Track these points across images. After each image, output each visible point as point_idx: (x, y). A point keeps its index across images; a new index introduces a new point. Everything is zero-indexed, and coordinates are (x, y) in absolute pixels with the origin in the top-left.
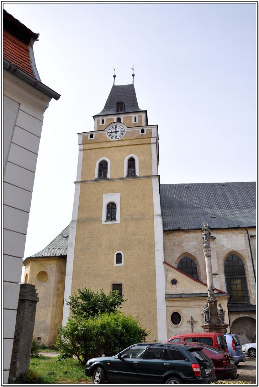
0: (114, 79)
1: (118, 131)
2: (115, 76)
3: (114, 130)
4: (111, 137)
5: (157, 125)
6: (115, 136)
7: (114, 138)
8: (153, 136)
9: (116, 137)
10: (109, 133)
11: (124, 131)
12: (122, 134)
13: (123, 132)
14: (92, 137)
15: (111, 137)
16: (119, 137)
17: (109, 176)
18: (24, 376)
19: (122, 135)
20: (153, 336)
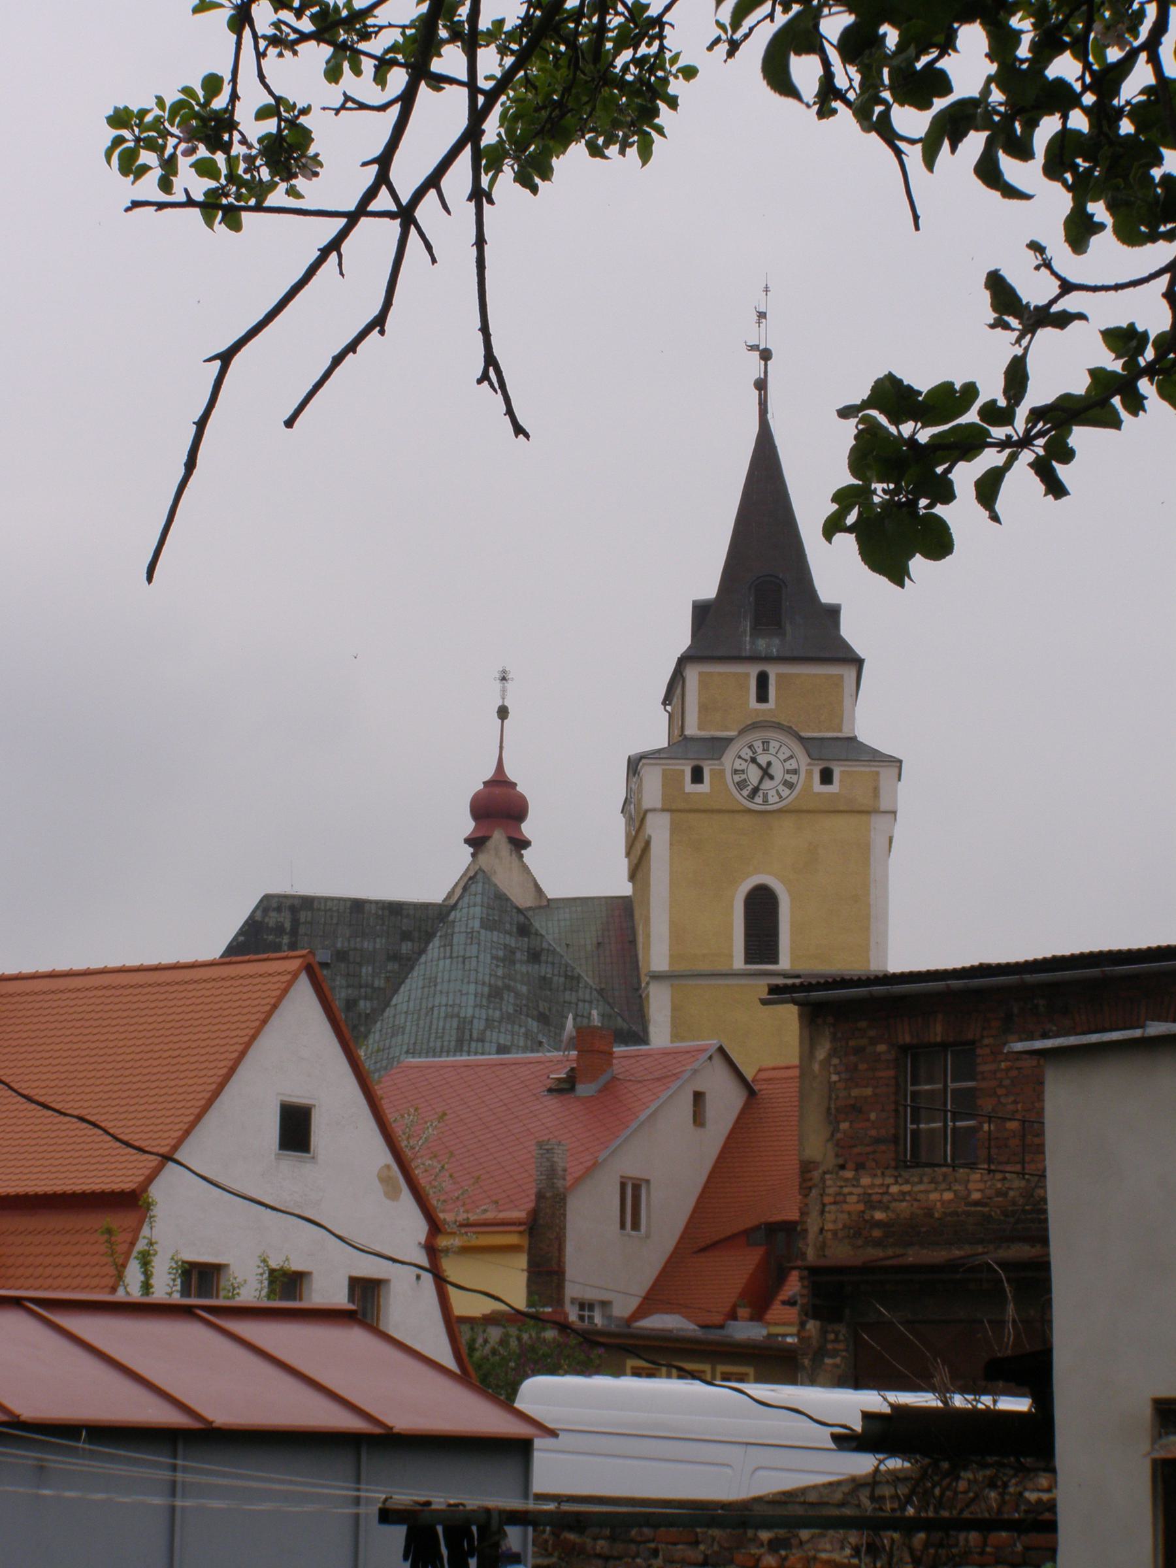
0: (766, 365)
1: (769, 764)
8: (882, 809)
19: (787, 792)
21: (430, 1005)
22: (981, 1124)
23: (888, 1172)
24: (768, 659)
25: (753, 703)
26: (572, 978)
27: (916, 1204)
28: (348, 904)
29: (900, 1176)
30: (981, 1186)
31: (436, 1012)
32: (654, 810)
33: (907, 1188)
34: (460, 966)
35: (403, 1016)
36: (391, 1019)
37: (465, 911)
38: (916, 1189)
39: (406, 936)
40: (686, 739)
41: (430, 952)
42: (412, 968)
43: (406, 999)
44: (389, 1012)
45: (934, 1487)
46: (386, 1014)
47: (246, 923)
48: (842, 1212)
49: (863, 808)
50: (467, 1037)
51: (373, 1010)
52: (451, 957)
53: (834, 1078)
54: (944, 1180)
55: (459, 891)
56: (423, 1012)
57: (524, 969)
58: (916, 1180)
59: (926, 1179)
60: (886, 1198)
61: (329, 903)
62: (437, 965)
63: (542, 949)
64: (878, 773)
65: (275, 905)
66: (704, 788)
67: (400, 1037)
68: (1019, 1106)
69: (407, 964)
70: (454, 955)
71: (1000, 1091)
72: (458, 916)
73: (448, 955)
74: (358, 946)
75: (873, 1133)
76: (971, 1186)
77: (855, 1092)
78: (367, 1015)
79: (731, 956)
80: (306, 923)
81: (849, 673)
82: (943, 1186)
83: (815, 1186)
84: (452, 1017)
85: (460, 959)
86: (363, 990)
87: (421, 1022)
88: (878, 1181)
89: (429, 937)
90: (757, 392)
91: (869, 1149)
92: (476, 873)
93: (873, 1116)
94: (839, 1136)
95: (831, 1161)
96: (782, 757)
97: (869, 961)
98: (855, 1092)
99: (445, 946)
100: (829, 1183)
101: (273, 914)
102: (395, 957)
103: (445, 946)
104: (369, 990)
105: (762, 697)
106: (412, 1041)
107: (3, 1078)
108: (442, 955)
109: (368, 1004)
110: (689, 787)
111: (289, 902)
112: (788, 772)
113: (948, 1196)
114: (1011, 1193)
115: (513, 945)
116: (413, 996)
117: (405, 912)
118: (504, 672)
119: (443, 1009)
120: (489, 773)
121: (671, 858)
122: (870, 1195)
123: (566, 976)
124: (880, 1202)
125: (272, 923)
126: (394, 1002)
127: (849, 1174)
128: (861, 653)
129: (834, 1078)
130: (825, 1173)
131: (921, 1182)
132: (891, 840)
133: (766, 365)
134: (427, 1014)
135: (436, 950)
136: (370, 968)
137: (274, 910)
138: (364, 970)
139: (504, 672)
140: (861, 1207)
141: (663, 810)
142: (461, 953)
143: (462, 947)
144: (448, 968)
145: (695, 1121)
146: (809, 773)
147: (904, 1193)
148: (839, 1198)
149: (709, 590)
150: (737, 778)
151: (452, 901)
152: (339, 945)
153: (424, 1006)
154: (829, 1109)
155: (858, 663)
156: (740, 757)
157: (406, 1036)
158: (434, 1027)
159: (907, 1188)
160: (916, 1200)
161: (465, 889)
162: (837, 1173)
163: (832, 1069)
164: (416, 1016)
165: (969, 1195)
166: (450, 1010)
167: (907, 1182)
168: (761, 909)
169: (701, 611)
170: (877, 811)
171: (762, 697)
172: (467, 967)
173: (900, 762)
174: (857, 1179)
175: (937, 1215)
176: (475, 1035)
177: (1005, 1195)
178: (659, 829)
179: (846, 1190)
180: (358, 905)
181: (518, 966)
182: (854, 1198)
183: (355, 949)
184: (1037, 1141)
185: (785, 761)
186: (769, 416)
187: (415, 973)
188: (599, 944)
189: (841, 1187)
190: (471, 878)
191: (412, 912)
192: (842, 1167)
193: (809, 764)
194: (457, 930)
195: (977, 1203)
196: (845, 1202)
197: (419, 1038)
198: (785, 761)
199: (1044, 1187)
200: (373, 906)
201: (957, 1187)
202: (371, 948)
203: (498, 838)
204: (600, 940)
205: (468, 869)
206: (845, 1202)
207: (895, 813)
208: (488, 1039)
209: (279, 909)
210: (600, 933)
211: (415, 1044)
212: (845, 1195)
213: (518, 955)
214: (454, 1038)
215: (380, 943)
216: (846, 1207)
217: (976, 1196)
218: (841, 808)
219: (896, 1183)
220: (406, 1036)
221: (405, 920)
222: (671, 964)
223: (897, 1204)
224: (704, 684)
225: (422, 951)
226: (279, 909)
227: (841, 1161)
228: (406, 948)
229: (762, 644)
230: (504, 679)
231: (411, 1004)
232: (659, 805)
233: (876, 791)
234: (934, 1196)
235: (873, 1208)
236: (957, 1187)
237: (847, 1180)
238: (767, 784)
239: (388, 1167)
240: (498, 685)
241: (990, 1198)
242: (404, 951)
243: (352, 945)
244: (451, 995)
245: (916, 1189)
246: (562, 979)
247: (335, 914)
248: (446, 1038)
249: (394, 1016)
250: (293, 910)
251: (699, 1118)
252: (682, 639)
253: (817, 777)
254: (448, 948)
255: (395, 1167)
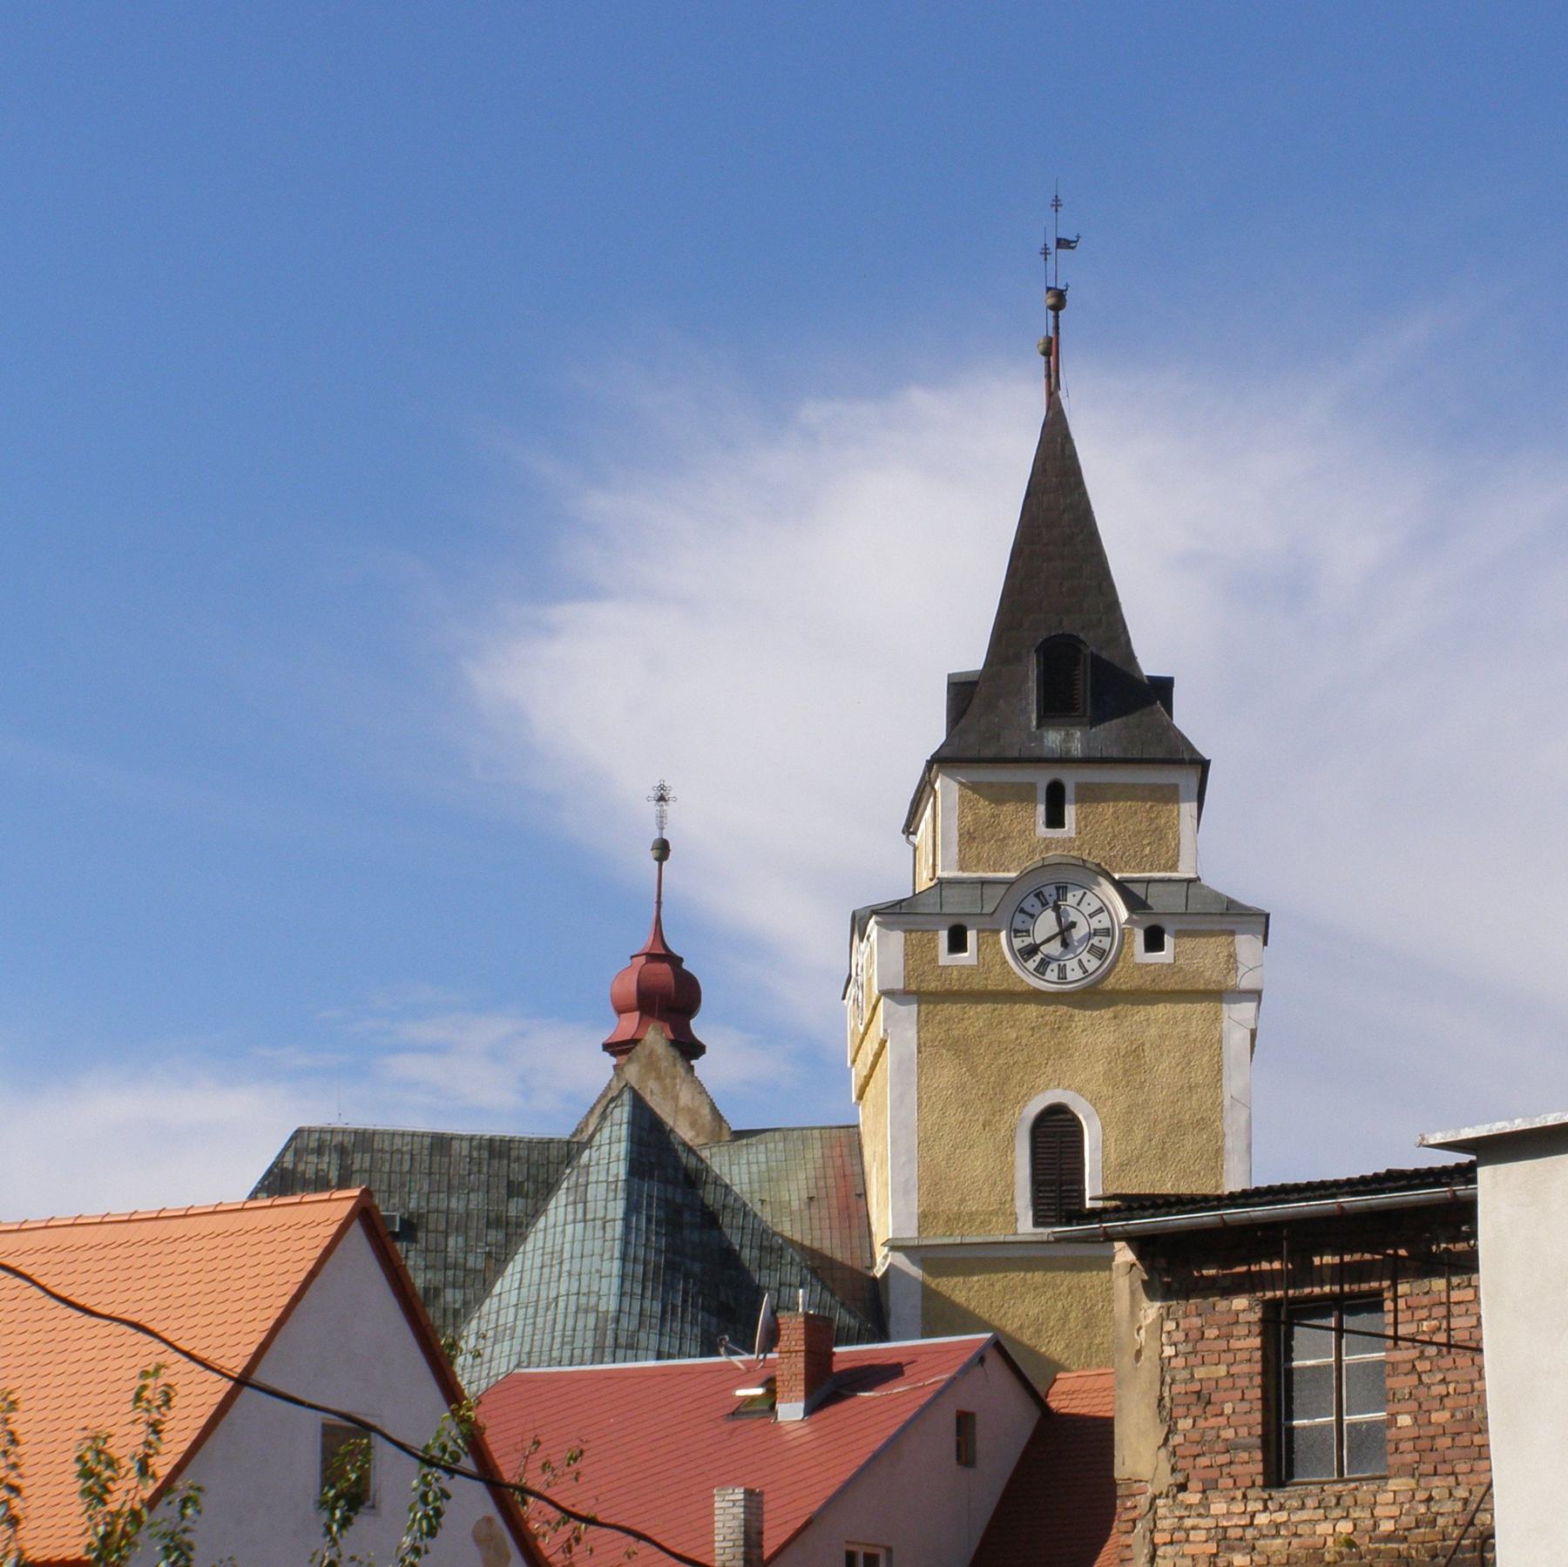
0: (1057, 317)
1: (1073, 925)
21: (553, 1294)
22: (1394, 1416)
23: (1251, 1493)
24: (1065, 760)
25: (1042, 831)
26: (771, 1250)
27: (1295, 1542)
28: (427, 1141)
29: (1271, 1498)
30: (1395, 1511)
31: (561, 1304)
33: (1281, 1517)
34: (599, 1233)
35: (512, 1311)
36: (493, 1316)
37: (605, 1149)
38: (1294, 1518)
39: (513, 1190)
41: (551, 1212)
42: (523, 1238)
43: (516, 1285)
44: (489, 1305)
46: (485, 1308)
47: (270, 1172)
48: (1183, 1556)
50: (609, 1341)
51: (466, 1303)
52: (585, 1221)
53: (1169, 1351)
54: (1338, 1504)
55: (594, 1121)
56: (542, 1304)
57: (696, 1236)
58: (1296, 1503)
59: (1310, 1502)
60: (1250, 1533)
61: (398, 1140)
62: (564, 1231)
63: (724, 1207)
65: (313, 1144)
66: (967, 957)
67: (507, 1344)
68: (1451, 1388)
69: (512, 1233)
70: (589, 1216)
71: (1422, 1366)
72: (595, 1155)
73: (580, 1215)
74: (443, 1206)
75: (1229, 1433)
76: (1378, 1511)
77: (1200, 1373)
78: (456, 1312)
80: (361, 1171)
81: (1185, 779)
82: (1337, 1513)
83: (1142, 1517)
84: (586, 1311)
85: (599, 1223)
86: (450, 1273)
87: (540, 1320)
88: (1238, 1507)
89: (548, 1189)
90: (1043, 359)
91: (1224, 1459)
92: (621, 1092)
93: (1228, 1409)
94: (1177, 1439)
95: (1166, 1479)
96: (1088, 910)
97: (1208, 1124)
98: (1200, 1373)
99: (575, 1203)
100: (1161, 1512)
101: (313, 1158)
102: (496, 1222)
103: (575, 1203)
104: (460, 1274)
105: (1055, 820)
106: (526, 1349)
107: (6, 1261)
108: (570, 1217)
109: (459, 1295)
110: (945, 958)
111: (338, 1139)
113: (1345, 1527)
114: (1441, 1521)
115: (679, 1199)
116: (526, 1282)
117: (514, 1154)
118: (662, 788)
119: (573, 1298)
120: (644, 941)
122: (1225, 1529)
123: (761, 1248)
124: (1241, 1539)
125: (310, 1173)
126: (497, 1289)
127: (1192, 1497)
128: (1204, 751)
129: (1169, 1351)
130: (1154, 1498)
131: (1303, 1507)
133: (1057, 317)
134: (547, 1309)
135: (561, 1210)
136: (461, 1240)
137: (312, 1151)
138: (451, 1242)
139: (662, 788)
140: (1212, 1548)
142: (600, 1214)
143: (601, 1204)
144: (579, 1235)
145: (959, 1457)
147: (1277, 1526)
148: (1179, 1535)
149: (972, 657)
151: (585, 1137)
152: (413, 1205)
153: (543, 1294)
154: (1161, 1399)
155: (1204, 765)
156: (1022, 911)
157: (517, 1341)
158: (559, 1326)
159: (1281, 1517)
160: (1296, 1535)
161: (603, 1117)
162: (1174, 1497)
163: (1164, 1339)
164: (531, 1311)
165: (1376, 1526)
166: (583, 1300)
167: (1281, 1508)
168: (1056, 1137)
169: (962, 692)
171: (1055, 820)
172: (609, 1236)
173: (1267, 916)
174: (1205, 1503)
175: (1328, 1557)
176: (622, 1341)
177: (1433, 1523)
179: (1188, 1523)
180: (441, 1143)
181: (686, 1232)
182: (1202, 1535)
183: (437, 1211)
184: (1477, 1439)
185: (1091, 916)
186: (1062, 394)
187: (529, 1246)
188: (811, 1199)
189: (1181, 1518)
190: (613, 1099)
191: (524, 1153)
192: (1183, 1487)
194: (592, 1178)
195: (1389, 1538)
196: (1187, 1540)
197: (537, 1344)
198: (1091, 916)
199: (1491, 1511)
200: (465, 1145)
201: (1355, 1513)
202: (462, 1209)
203: (656, 1038)
204: (813, 1193)
205: (609, 1087)
206: (1187, 1540)
208: (643, 1344)
209: (319, 1151)
210: (812, 1183)
211: (529, 1353)
212: (1187, 1531)
213: (687, 1217)
214: (590, 1344)
215: (477, 1200)
216: (1188, 1549)
217: (1387, 1526)
219: (1266, 1508)
220: (517, 1341)
221: (515, 1166)
223: (1268, 1542)
225: (536, 1213)
226: (319, 1151)
227: (1180, 1478)
228: (515, 1208)
229: (1053, 739)
230: (662, 799)
231: (524, 1291)
234: (1324, 1528)
235: (1231, 1549)
236: (1355, 1513)
237: (1189, 1507)
239: (489, 1520)
240: (653, 807)
241: (1409, 1529)
242: (512, 1213)
243: (433, 1205)
244: (585, 1279)
245: (1294, 1518)
246: (756, 1253)
247: (407, 1157)
248: (579, 1343)
249: (498, 1312)
250: (342, 1150)
251: (965, 1454)
252: (934, 733)
254: (580, 1206)
255: (499, 1521)
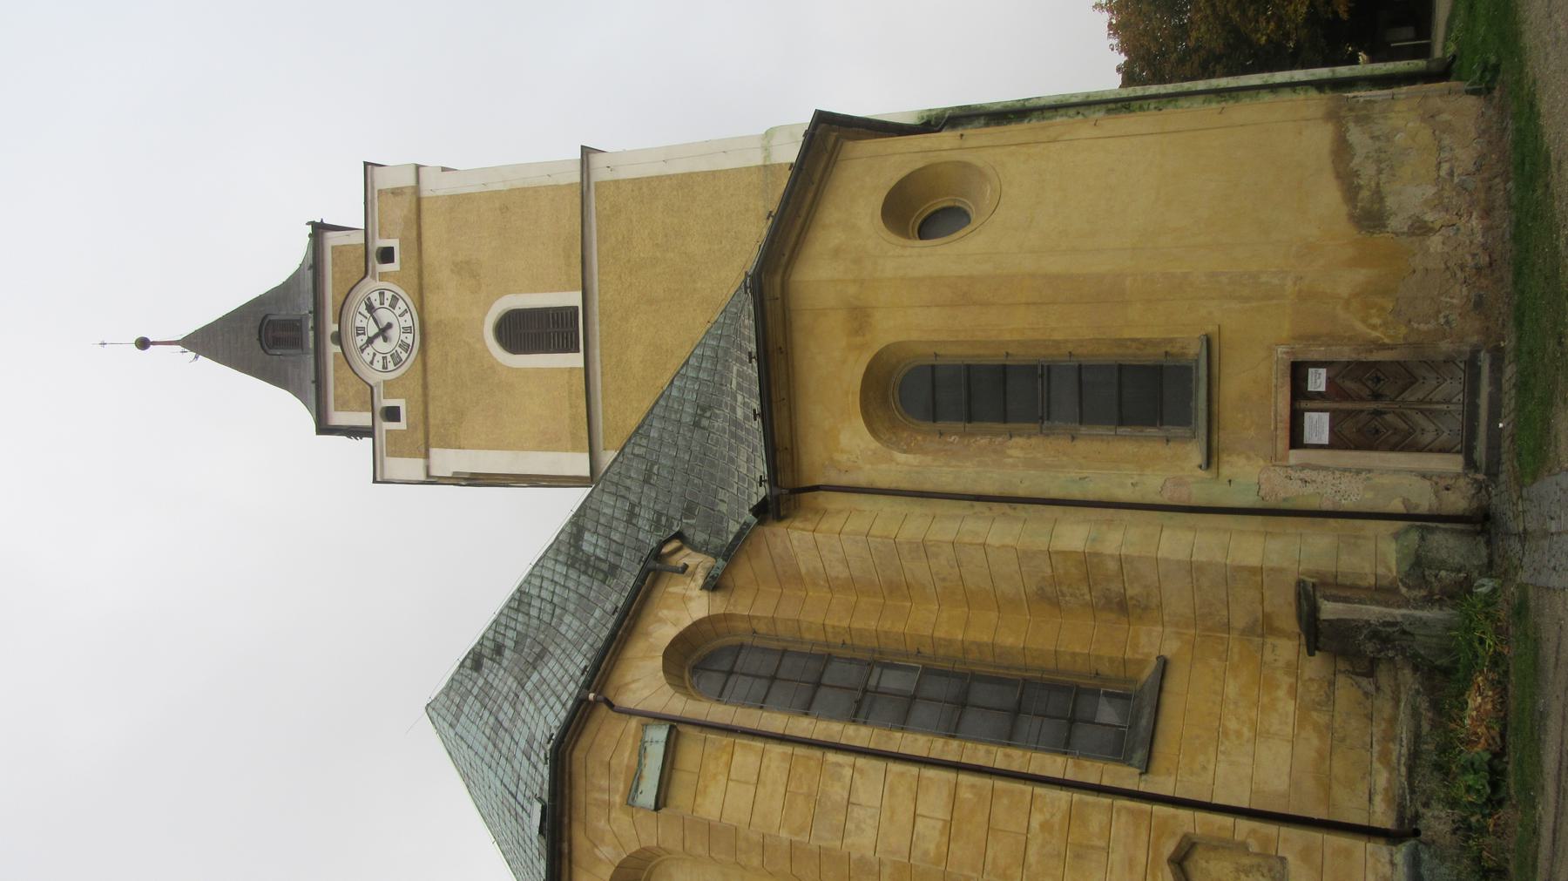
0: (155, 343)
1: (389, 326)
2: (143, 344)
3: (372, 330)
4: (404, 355)
5: (375, 481)
6: (403, 337)
7: (409, 339)
8: (412, 182)
9: (407, 330)
10: (385, 367)
11: (381, 294)
12: (395, 299)
13: (388, 295)
14: (397, 408)
15: (404, 355)
16: (410, 336)
17: (574, 299)
18: (1431, 594)
19: (401, 304)
20: (1163, 55)
32: (428, 469)
40: (1154, 75)
45: (733, 409)
49: (414, 206)
64: (380, 191)
79: (571, 370)
112: (393, 306)
121: (473, 447)
132: (444, 169)
133: (155, 343)
141: (427, 456)
146: (383, 277)
150: (391, 366)
170: (417, 188)
173: (823, 120)
178: (447, 460)
193: (373, 277)
207: (418, 167)
218: (414, 234)
222: (582, 451)
224: (343, 406)
232: (420, 462)
233: (396, 192)
238: (379, 342)
253: (387, 267)
